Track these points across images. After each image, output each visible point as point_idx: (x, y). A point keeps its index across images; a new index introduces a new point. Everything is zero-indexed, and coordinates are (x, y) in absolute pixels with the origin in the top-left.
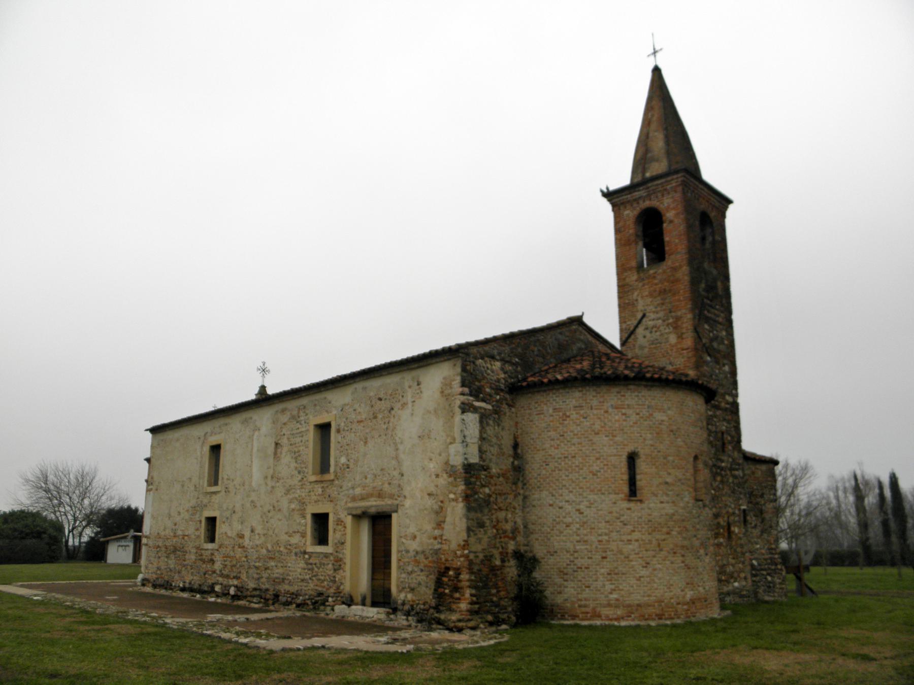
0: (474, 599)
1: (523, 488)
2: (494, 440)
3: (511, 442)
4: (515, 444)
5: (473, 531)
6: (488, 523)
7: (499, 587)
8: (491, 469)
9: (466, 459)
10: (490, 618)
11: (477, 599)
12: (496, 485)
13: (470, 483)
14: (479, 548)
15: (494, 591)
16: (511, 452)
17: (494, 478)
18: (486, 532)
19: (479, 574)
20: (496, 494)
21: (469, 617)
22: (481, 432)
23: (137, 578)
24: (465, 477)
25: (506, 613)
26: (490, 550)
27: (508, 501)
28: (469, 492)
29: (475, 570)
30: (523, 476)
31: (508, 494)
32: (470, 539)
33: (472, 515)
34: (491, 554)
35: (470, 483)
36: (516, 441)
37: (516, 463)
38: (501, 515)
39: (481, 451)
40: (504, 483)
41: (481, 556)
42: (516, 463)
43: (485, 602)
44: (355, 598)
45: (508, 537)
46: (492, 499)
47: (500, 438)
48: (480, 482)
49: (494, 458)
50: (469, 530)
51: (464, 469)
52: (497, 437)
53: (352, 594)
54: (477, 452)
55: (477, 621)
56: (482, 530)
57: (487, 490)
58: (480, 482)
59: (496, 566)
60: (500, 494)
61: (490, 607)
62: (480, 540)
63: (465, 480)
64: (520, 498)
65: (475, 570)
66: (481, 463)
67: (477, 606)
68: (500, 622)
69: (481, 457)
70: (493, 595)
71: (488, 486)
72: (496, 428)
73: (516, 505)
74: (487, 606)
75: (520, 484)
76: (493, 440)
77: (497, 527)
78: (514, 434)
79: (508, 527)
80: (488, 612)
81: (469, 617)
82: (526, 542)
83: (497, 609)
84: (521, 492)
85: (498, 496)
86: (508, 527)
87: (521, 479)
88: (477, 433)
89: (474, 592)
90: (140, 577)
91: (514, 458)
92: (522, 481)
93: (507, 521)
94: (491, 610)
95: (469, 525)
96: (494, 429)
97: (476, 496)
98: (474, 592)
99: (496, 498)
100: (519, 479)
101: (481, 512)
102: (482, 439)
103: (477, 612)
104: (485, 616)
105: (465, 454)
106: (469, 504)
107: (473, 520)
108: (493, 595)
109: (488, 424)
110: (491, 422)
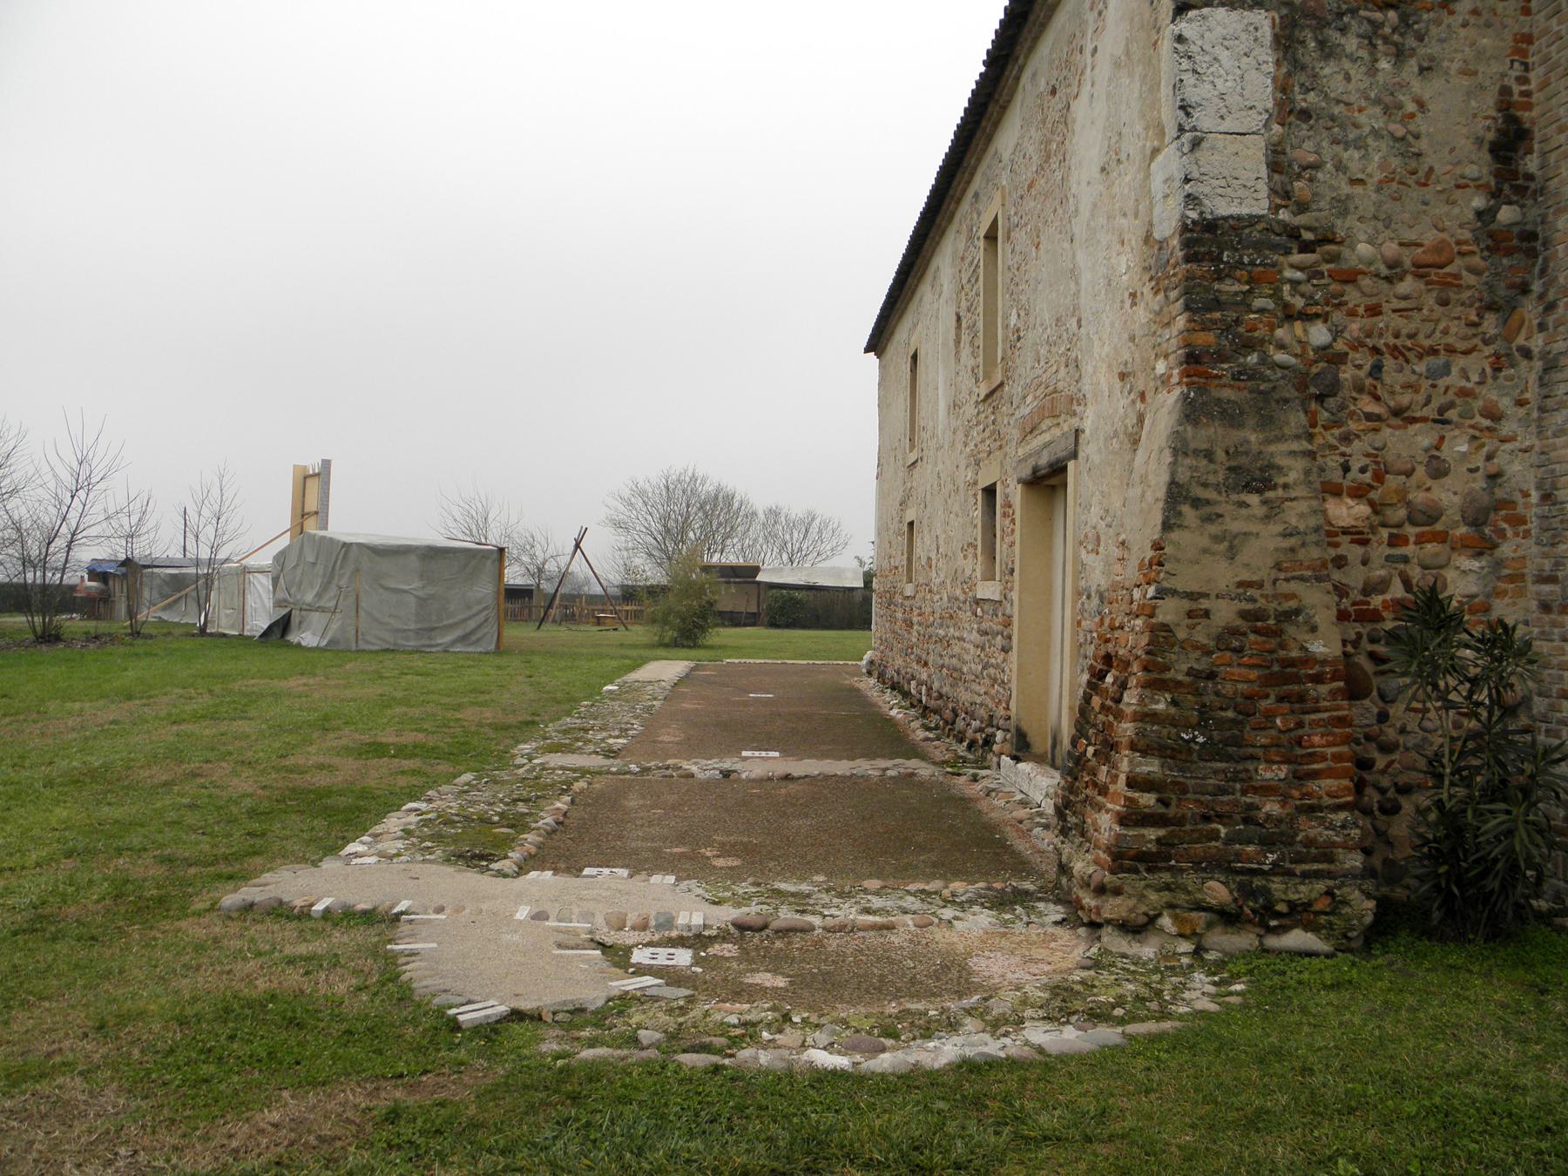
0: (1148, 800)
1: (1542, 327)
2: (1371, 118)
3: (1486, 125)
4: (1502, 133)
5: (1197, 503)
6: (1294, 471)
7: (1313, 757)
8: (1348, 241)
9: (1191, 199)
10: (1218, 891)
11: (1164, 802)
12: (1374, 311)
13: (1217, 304)
14: (1223, 575)
15: (1273, 773)
16: (1479, 166)
17: (1366, 282)
18: (1273, 511)
19: (1198, 693)
20: (1375, 350)
21: (1108, 878)
22: (1283, 87)
23: (862, 659)
24: (1189, 277)
25: (1330, 875)
26: (1284, 587)
27: (1454, 379)
28: (1206, 339)
29: (1179, 673)
30: (1543, 272)
31: (1451, 350)
32: (1175, 535)
33: (1210, 433)
34: (1293, 604)
35: (1217, 304)
36: (1512, 120)
37: (1506, 214)
38: (1413, 442)
39: (1277, 162)
40: (1430, 301)
41: (1225, 613)
42: (1506, 214)
43: (1206, 819)
44: (1033, 737)
45: (1441, 537)
46: (1347, 374)
47: (1411, 107)
48: (1276, 295)
49: (1366, 198)
50: (1176, 495)
51: (1187, 244)
52: (1390, 109)
53: (1025, 727)
54: (1264, 171)
55: (1142, 897)
56: (1254, 499)
57: (1319, 334)
58: (1276, 295)
59: (1308, 659)
60: (1396, 351)
61: (1229, 841)
62: (1232, 547)
63: (1187, 292)
64: (1529, 372)
65: (1179, 673)
66: (1283, 215)
67: (1152, 834)
68: (1278, 915)
69: (1282, 195)
70: (1267, 790)
71: (1325, 317)
72: (1384, 65)
73: (1505, 403)
74: (1214, 836)
75: (1530, 309)
76: (1362, 119)
77: (1373, 495)
78: (1505, 91)
79: (1449, 495)
80: (1219, 865)
81: (1108, 878)
82: (1547, 565)
83: (1271, 857)
84: (1537, 343)
85: (1389, 362)
86: (1449, 495)
87: (1536, 287)
88: (1261, 91)
89: (1151, 767)
90: (868, 655)
91: (1496, 194)
92: (1541, 297)
93: (1438, 470)
94: (1238, 857)
95: (1183, 476)
96: (1373, 71)
97: (1253, 359)
98: (1151, 767)
99: (1377, 370)
100: (1525, 289)
101: (1266, 421)
102: (1288, 111)
103: (1149, 861)
104: (1190, 879)
105: (1187, 180)
106: (1202, 390)
107: (1209, 455)
108: (1267, 790)
109: (1328, 51)
110: (1351, 44)
